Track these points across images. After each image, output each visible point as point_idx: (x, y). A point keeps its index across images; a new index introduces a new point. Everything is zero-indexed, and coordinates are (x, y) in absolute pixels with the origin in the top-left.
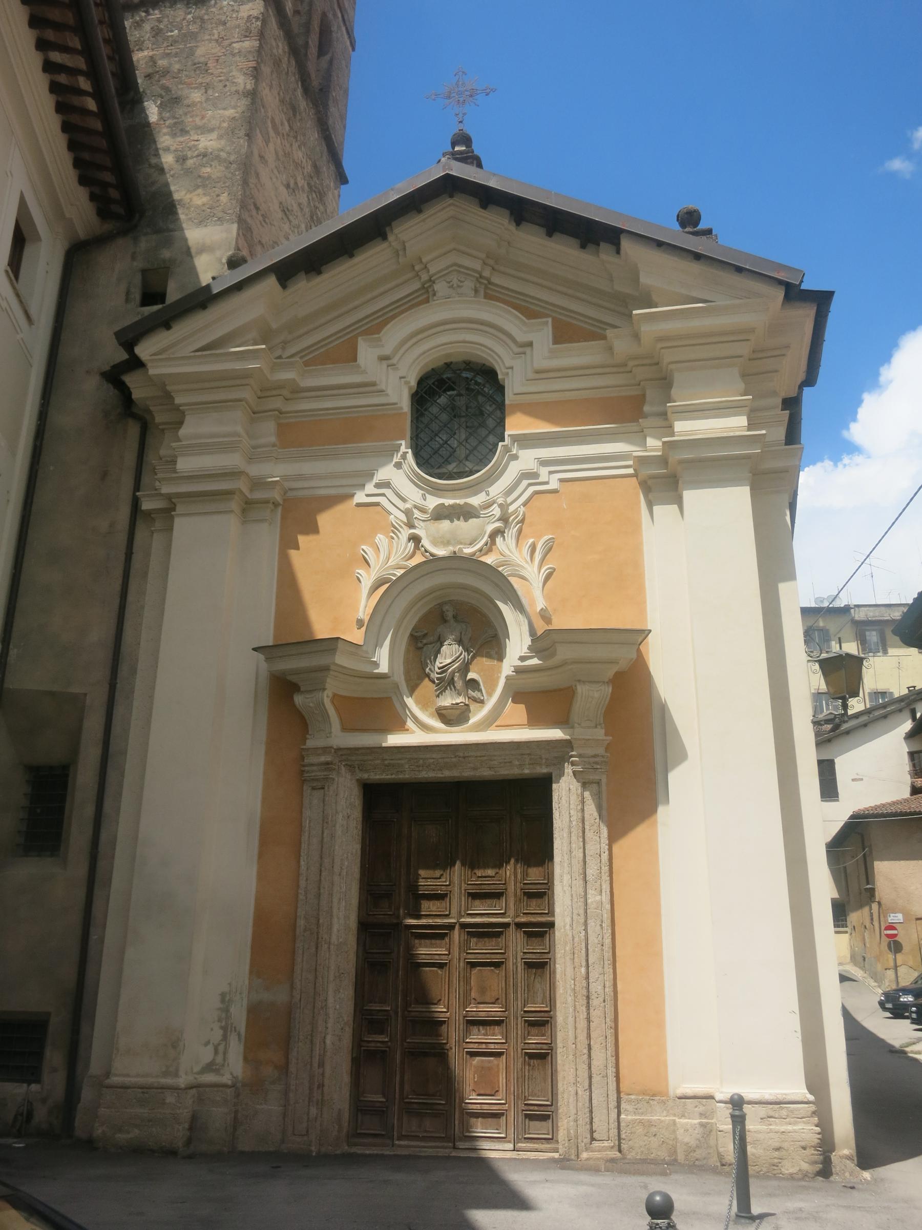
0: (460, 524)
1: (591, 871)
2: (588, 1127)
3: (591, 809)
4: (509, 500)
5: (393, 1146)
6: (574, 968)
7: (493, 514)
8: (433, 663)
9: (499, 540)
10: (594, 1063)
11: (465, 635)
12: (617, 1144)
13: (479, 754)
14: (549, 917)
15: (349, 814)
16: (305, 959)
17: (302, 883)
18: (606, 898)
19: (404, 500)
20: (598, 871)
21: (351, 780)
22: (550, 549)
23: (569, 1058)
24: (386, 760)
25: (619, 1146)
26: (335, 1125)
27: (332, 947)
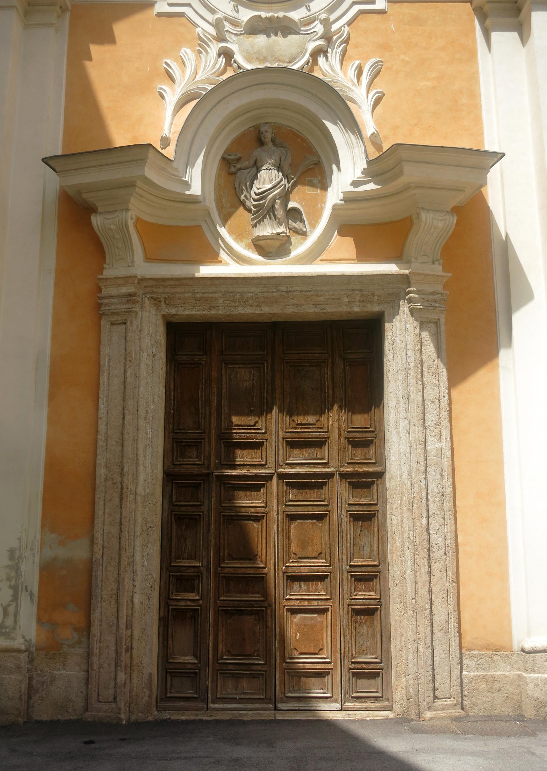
0: (278, 40)
1: (431, 417)
2: (431, 685)
3: (429, 349)
4: (332, 18)
5: (207, 709)
6: (413, 519)
7: (315, 31)
8: (249, 190)
9: (321, 60)
10: (436, 618)
11: (285, 159)
12: (460, 702)
13: (304, 288)
14: (377, 467)
15: (155, 352)
16: (107, 511)
17: (102, 427)
18: (445, 445)
19: (212, 11)
20: (438, 417)
21: (156, 315)
22: (378, 73)
23: (408, 613)
24: (198, 293)
25: (462, 703)
26: (145, 690)
27: (139, 498)
